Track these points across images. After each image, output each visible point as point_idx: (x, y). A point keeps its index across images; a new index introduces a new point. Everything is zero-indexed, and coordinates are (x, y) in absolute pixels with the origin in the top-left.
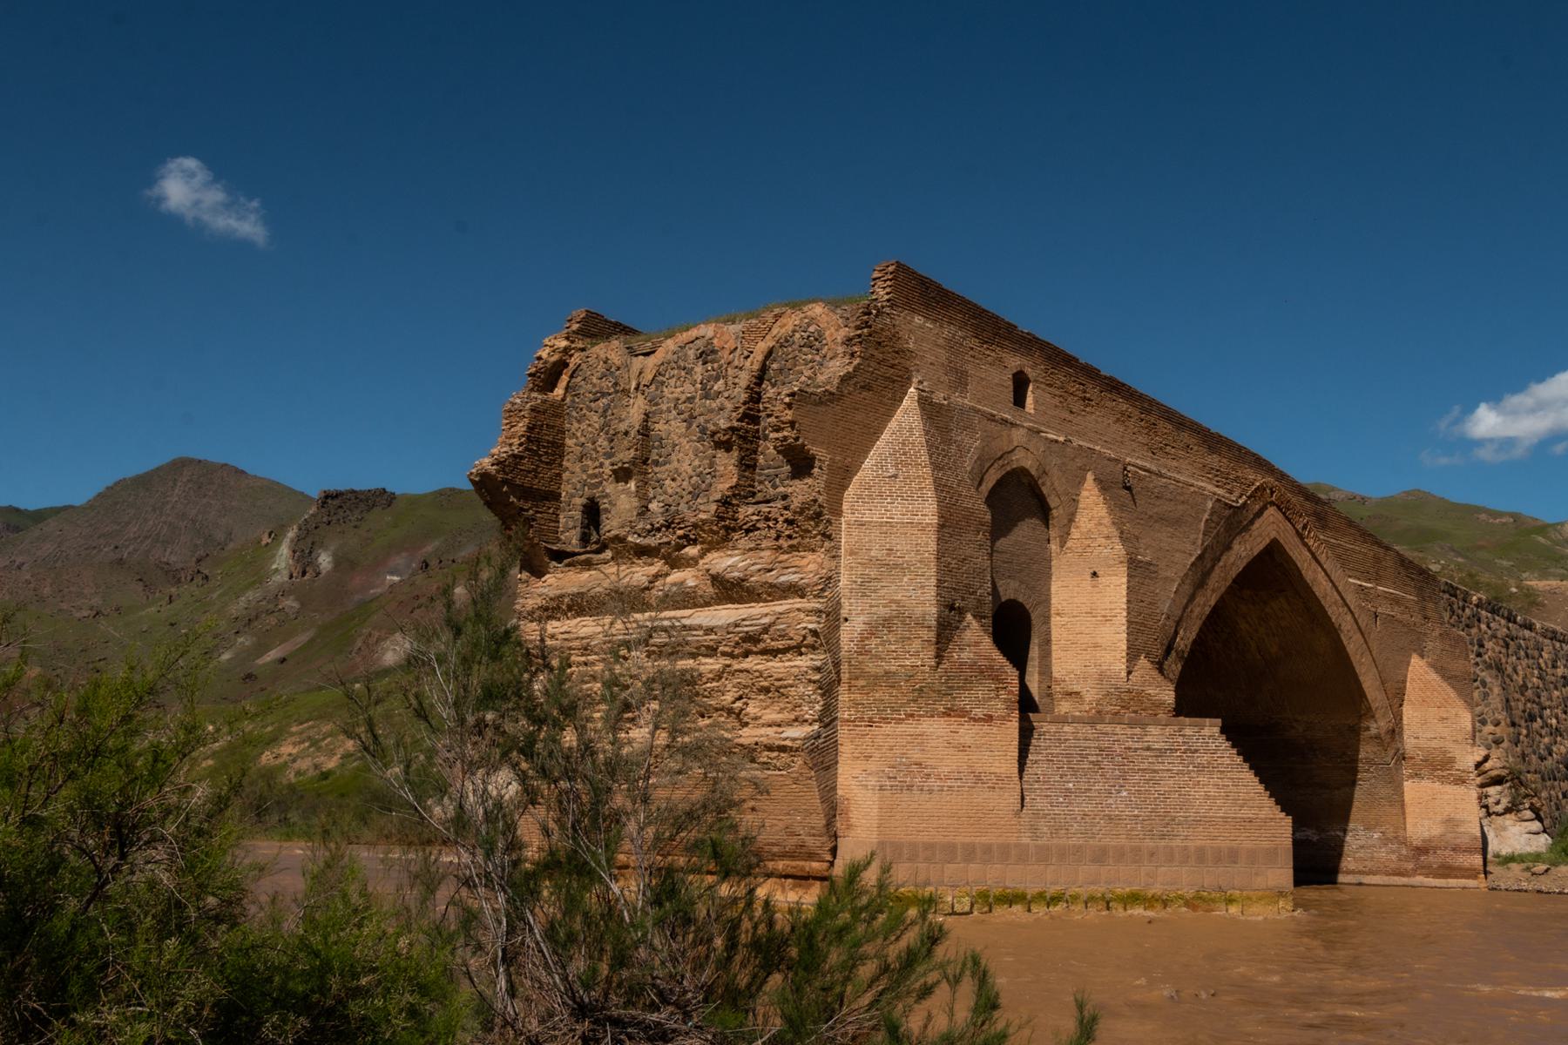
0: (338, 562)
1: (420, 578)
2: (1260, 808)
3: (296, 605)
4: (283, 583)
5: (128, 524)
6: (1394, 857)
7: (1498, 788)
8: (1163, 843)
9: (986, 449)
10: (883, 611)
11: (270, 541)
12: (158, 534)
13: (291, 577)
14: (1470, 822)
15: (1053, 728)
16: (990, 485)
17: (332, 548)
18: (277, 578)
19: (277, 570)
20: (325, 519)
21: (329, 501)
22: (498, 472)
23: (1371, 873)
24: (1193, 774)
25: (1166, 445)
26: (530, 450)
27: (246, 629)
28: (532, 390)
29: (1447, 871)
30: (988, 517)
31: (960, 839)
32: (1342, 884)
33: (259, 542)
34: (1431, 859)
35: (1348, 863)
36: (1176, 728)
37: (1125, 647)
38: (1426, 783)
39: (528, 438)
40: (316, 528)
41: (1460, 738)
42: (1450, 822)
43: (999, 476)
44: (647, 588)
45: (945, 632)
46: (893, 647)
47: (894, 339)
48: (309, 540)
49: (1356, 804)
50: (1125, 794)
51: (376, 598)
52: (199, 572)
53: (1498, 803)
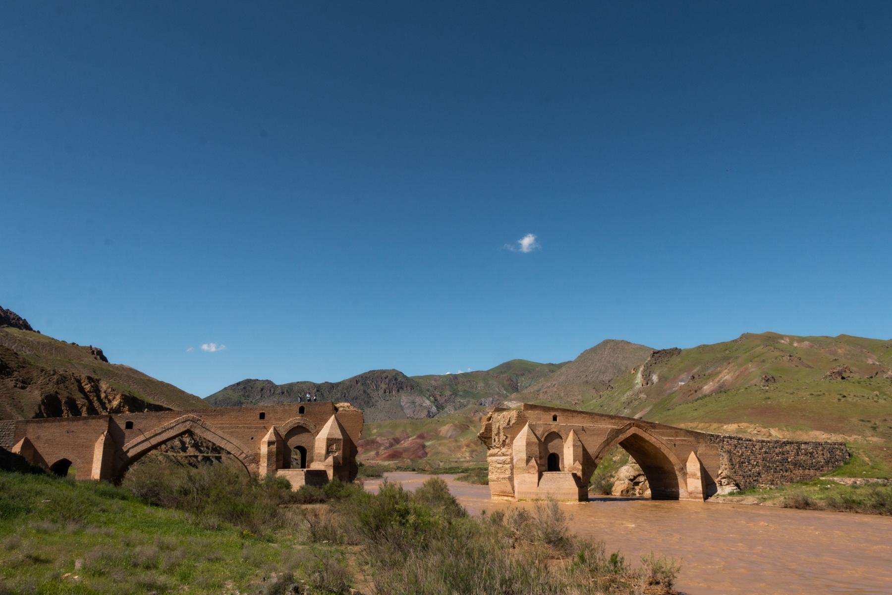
0: (660, 379)
1: (691, 383)
3: (645, 396)
5: (589, 366)
7: (725, 479)
13: (643, 385)
18: (637, 386)
19: (637, 383)
20: (654, 362)
21: (655, 355)
35: (680, 496)
40: (651, 366)
42: (696, 487)
48: (648, 371)
51: (675, 392)
53: (724, 483)
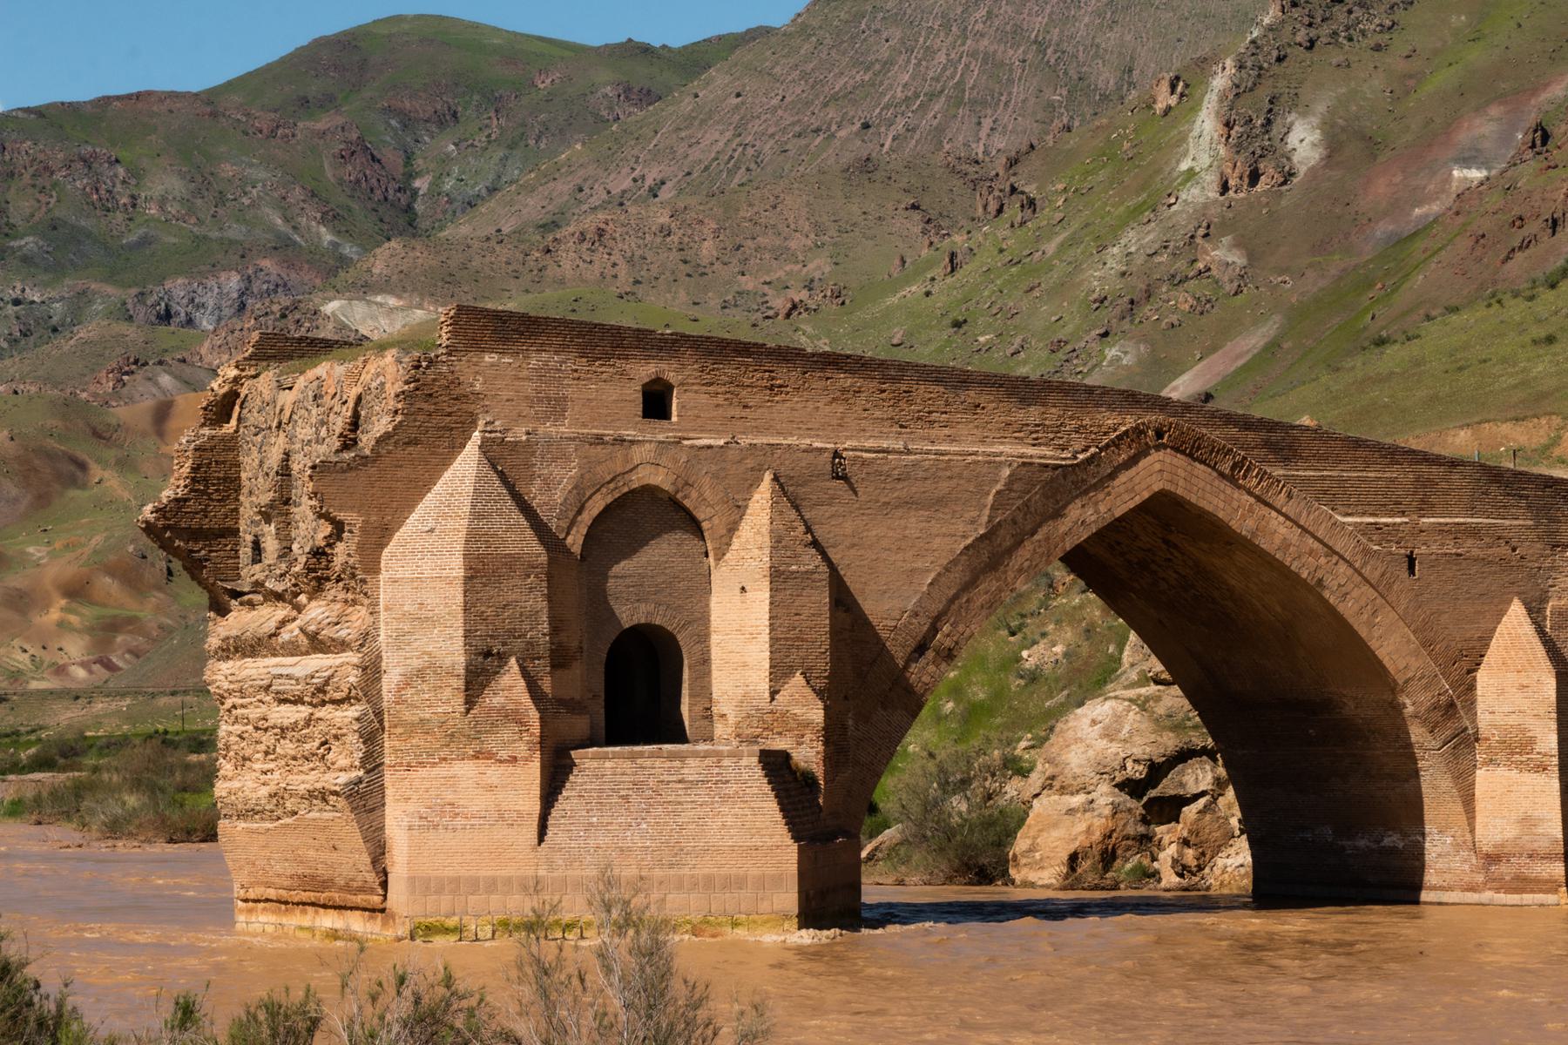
0: (1333, 144)
1: (1528, 173)
2: (771, 836)
3: (1237, 258)
4: (1205, 206)
5: (888, 64)
6: (1467, 867)
8: (672, 872)
9: (587, 476)
10: (416, 663)
11: (1173, 100)
12: (960, 85)
13: (1225, 188)
14: (1550, 820)
15: (595, 764)
16: (595, 512)
17: (1321, 108)
20: (1301, 37)
22: (157, 519)
23: (1450, 889)
24: (716, 805)
25: (930, 412)
26: (196, 491)
27: (1126, 325)
28: (203, 425)
29: (1522, 884)
30: (544, 559)
31: (483, 873)
32: (1426, 903)
33: (1149, 107)
34: (1504, 870)
35: (1430, 877)
36: (715, 759)
37: (768, 666)
38: (1501, 772)
39: (193, 479)
41: (1542, 712)
42: (1527, 821)
43: (609, 499)
44: (275, 635)
45: (477, 680)
46: (427, 696)
47: (452, 387)
48: (1264, 93)
49: (1426, 800)
50: (644, 826)
52: (1013, 190)
